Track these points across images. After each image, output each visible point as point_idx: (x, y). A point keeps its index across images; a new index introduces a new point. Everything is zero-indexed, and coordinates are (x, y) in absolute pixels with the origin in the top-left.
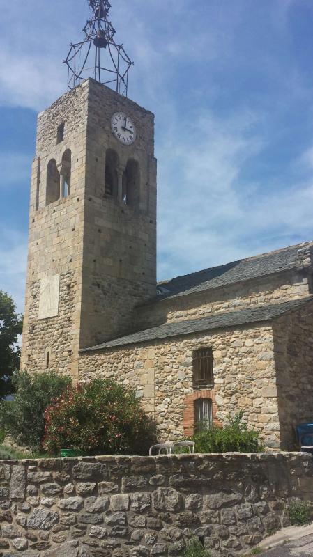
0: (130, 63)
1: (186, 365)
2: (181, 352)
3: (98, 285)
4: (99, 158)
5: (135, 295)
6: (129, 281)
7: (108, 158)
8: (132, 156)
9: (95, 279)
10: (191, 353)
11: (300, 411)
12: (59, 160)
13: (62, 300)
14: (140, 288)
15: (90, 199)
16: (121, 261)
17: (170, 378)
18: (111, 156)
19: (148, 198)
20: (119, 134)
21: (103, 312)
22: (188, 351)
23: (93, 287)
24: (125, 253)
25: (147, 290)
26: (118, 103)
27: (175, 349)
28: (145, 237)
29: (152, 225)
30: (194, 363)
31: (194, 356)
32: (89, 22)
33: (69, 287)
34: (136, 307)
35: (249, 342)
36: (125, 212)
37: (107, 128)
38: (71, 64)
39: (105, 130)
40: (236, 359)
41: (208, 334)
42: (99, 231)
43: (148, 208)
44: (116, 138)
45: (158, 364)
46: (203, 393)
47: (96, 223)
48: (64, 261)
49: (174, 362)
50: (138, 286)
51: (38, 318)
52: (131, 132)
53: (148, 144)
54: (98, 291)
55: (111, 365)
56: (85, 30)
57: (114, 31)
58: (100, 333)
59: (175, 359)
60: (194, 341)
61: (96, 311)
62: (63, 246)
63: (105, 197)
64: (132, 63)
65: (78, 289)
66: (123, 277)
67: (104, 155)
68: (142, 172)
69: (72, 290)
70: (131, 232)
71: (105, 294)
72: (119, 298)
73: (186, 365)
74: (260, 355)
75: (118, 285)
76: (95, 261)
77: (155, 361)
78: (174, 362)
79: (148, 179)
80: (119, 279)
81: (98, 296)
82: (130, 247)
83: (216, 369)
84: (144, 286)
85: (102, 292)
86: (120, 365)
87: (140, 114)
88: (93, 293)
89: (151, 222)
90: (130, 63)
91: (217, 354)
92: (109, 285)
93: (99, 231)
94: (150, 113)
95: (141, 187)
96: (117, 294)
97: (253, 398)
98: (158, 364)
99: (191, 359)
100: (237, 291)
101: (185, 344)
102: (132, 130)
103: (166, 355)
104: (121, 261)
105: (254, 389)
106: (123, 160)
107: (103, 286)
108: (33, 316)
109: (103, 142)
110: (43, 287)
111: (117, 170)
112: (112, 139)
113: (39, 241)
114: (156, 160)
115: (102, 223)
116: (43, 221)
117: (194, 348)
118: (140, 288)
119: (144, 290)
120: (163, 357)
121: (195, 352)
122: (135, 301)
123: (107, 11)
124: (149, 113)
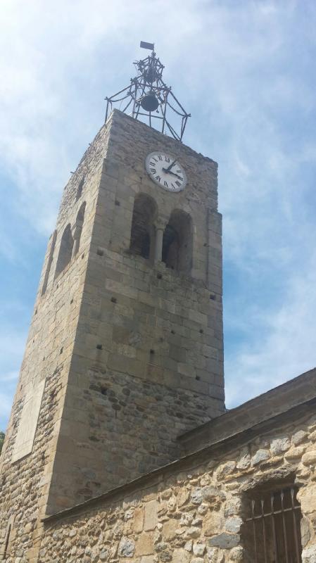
0: (186, 116)
2: (215, 503)
4: (123, 203)
5: (180, 416)
6: (169, 389)
7: (137, 214)
8: (179, 207)
9: (96, 377)
14: (191, 404)
15: (100, 253)
16: (152, 352)
18: (145, 207)
19: (208, 262)
20: (158, 177)
21: (108, 442)
22: (228, 495)
23: (91, 391)
24: (162, 340)
26: (159, 143)
27: (198, 494)
28: (203, 319)
29: (215, 302)
30: (246, 535)
31: (244, 512)
34: (180, 438)
36: (164, 277)
37: (139, 168)
39: (136, 171)
41: (279, 433)
42: (114, 300)
43: (207, 278)
44: (154, 183)
45: (162, 544)
47: (107, 287)
49: (194, 536)
50: (187, 398)
52: (179, 178)
53: (207, 196)
55: (80, 551)
58: (98, 485)
59: (199, 524)
60: (242, 463)
61: (93, 439)
63: (129, 253)
64: (190, 115)
65: (61, 397)
66: (155, 380)
67: (132, 200)
68: (196, 229)
70: (174, 309)
71: (116, 408)
72: (146, 418)
75: (145, 393)
76: (99, 347)
77: (157, 535)
78: (194, 536)
79: (208, 238)
80: (147, 384)
81: (100, 410)
82: (172, 332)
84: (197, 399)
85: (110, 404)
88: (89, 404)
89: (213, 298)
90: (186, 116)
92: (127, 392)
93: (114, 300)
94: (211, 161)
95: (195, 247)
96: (142, 410)
98: (162, 544)
99: (235, 523)
101: (221, 477)
102: (181, 175)
103: (178, 517)
104: (152, 352)
106: (165, 210)
107: (113, 394)
109: (132, 183)
111: (155, 223)
112: (146, 182)
115: (124, 290)
117: (244, 485)
118: (191, 404)
119: (199, 407)
120: (173, 521)
121: (247, 496)
122: (180, 426)
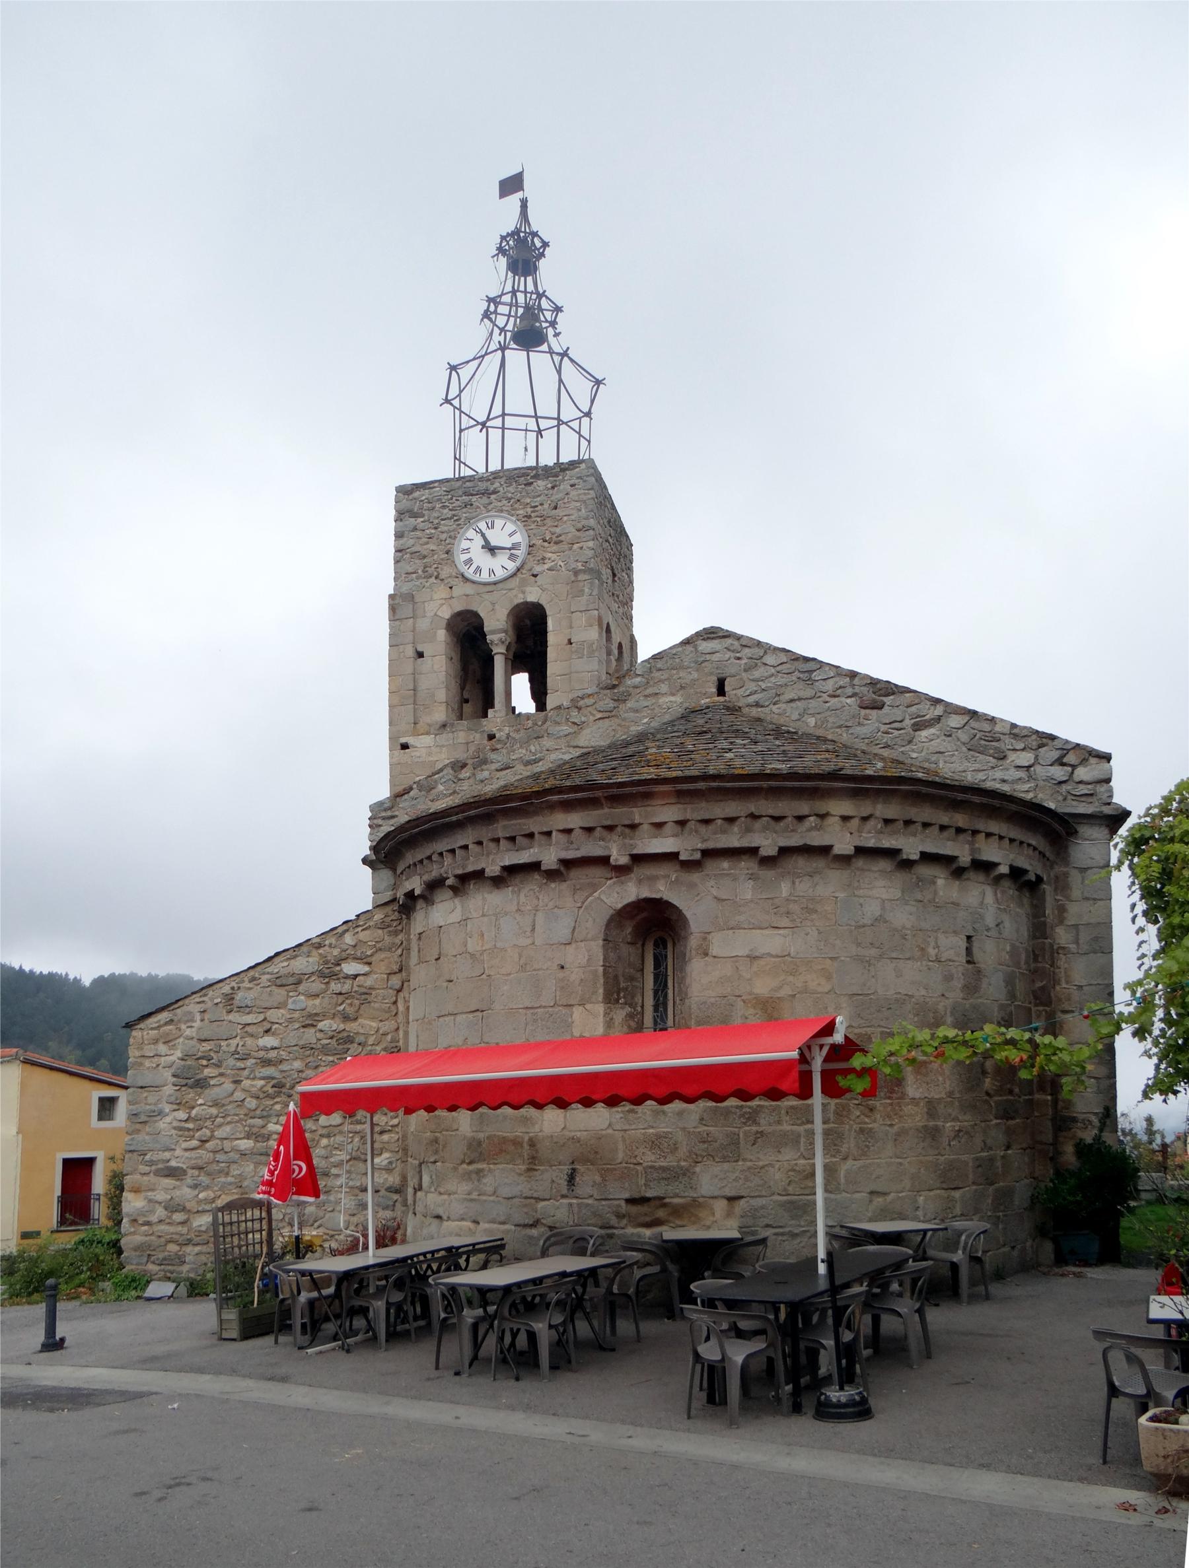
0: (598, 383)
8: (520, 600)
44: (474, 582)
106: (497, 626)
112: (460, 589)
123: (542, 255)
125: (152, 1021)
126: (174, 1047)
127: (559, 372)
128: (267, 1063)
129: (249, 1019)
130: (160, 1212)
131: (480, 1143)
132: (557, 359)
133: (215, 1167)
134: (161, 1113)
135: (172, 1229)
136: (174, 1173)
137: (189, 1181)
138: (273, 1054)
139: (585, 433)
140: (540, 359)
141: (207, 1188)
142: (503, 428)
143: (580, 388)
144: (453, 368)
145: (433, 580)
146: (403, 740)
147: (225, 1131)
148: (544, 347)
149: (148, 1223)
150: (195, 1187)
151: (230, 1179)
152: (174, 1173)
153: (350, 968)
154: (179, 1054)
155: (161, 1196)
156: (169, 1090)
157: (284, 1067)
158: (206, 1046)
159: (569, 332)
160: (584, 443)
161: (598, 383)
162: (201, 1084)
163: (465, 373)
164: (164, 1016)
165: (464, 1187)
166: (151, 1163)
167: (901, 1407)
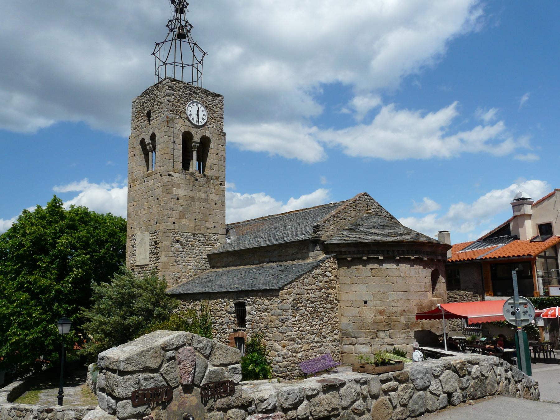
0: (205, 53)
1: (230, 313)
3: (178, 241)
10: (234, 305)
11: (300, 346)
12: (148, 141)
13: (152, 253)
17: (220, 321)
25: (218, 240)
32: (170, 21)
33: (156, 243)
35: (267, 302)
38: (157, 55)
40: (259, 313)
42: (178, 199)
46: (239, 334)
47: (174, 193)
48: (152, 223)
51: (135, 264)
54: (178, 246)
56: (168, 26)
57: (191, 27)
58: (179, 278)
62: (151, 211)
67: (181, 137)
69: (158, 246)
72: (194, 249)
73: (230, 313)
74: (272, 312)
76: (174, 223)
83: (247, 318)
86: (190, 307)
87: (210, 98)
91: (248, 308)
94: (221, 96)
97: (268, 340)
100: (275, 250)
105: (268, 334)
106: (197, 138)
107: (181, 242)
108: (132, 262)
110: (138, 240)
113: (135, 203)
114: (225, 134)
116: (138, 187)
122: (208, 250)
124: (219, 96)
125: (286, 288)
126: (291, 297)
127: (193, 52)
128: (312, 302)
129: (307, 288)
130: (290, 353)
131: (408, 324)
132: (192, 45)
133: (302, 337)
134: (289, 319)
135: (293, 358)
136: (293, 340)
137: (297, 342)
138: (314, 300)
139: (200, 69)
140: (185, 45)
141: (301, 344)
142: (175, 65)
143: (199, 55)
144: (157, 44)
145: (178, 116)
146: (170, 173)
147: (303, 325)
148: (186, 40)
149: (288, 358)
150: (297, 344)
151: (306, 340)
152: (293, 340)
153: (328, 274)
154: (292, 299)
155: (290, 347)
156: (290, 311)
157: (316, 303)
158: (298, 296)
159: (194, 35)
160: (199, 74)
161: (205, 53)
162: (298, 309)
163: (160, 45)
164: (289, 286)
165: (404, 336)
166: (287, 336)
167: (19, 400)
